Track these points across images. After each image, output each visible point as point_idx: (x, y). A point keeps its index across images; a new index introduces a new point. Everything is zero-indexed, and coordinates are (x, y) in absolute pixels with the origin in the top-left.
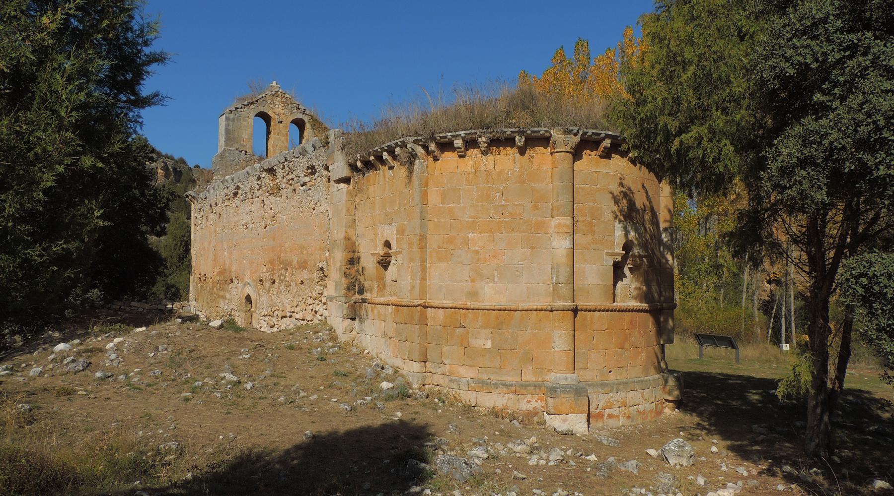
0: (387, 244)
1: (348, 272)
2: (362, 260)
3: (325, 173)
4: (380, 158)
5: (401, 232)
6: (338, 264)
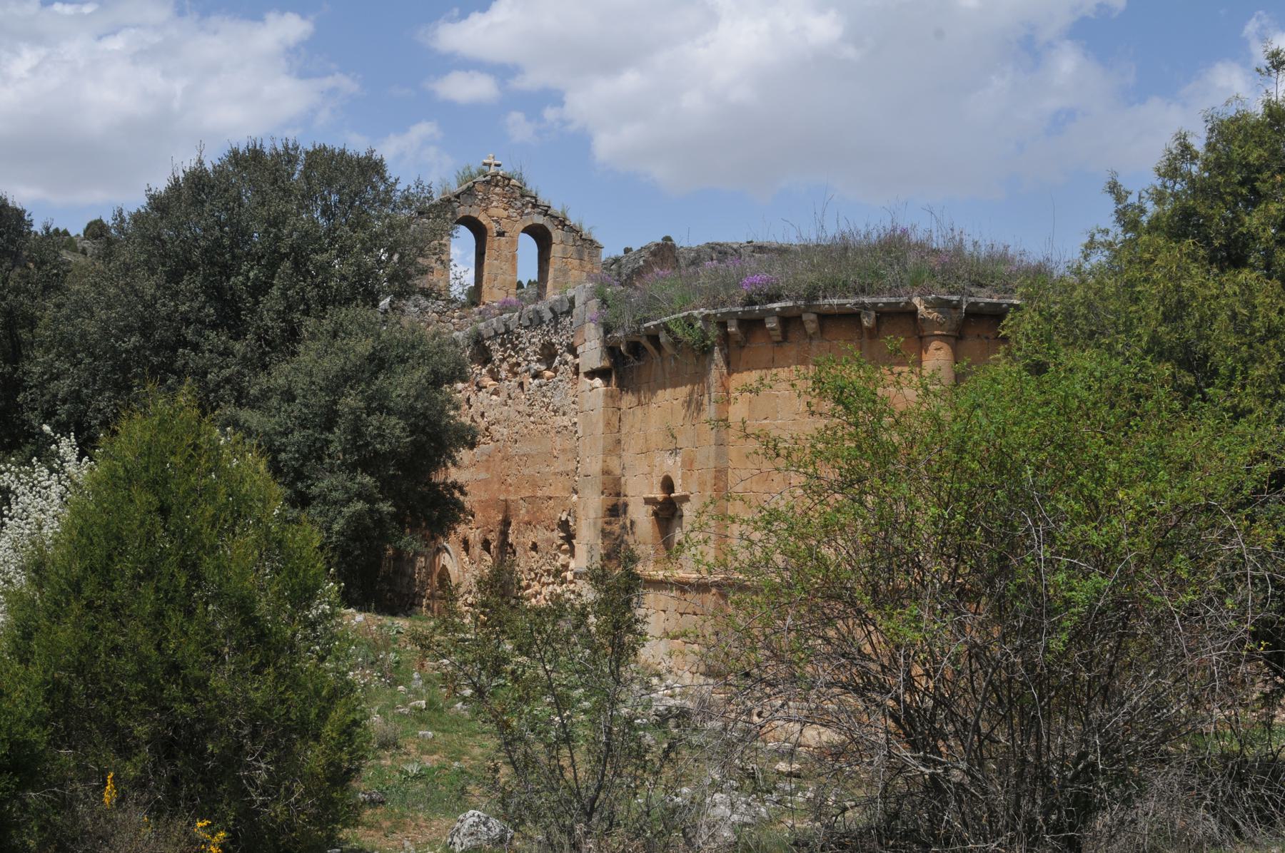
0: (668, 485)
1: (608, 528)
2: (631, 509)
3: (570, 358)
4: (654, 339)
5: (689, 465)
6: (592, 515)
